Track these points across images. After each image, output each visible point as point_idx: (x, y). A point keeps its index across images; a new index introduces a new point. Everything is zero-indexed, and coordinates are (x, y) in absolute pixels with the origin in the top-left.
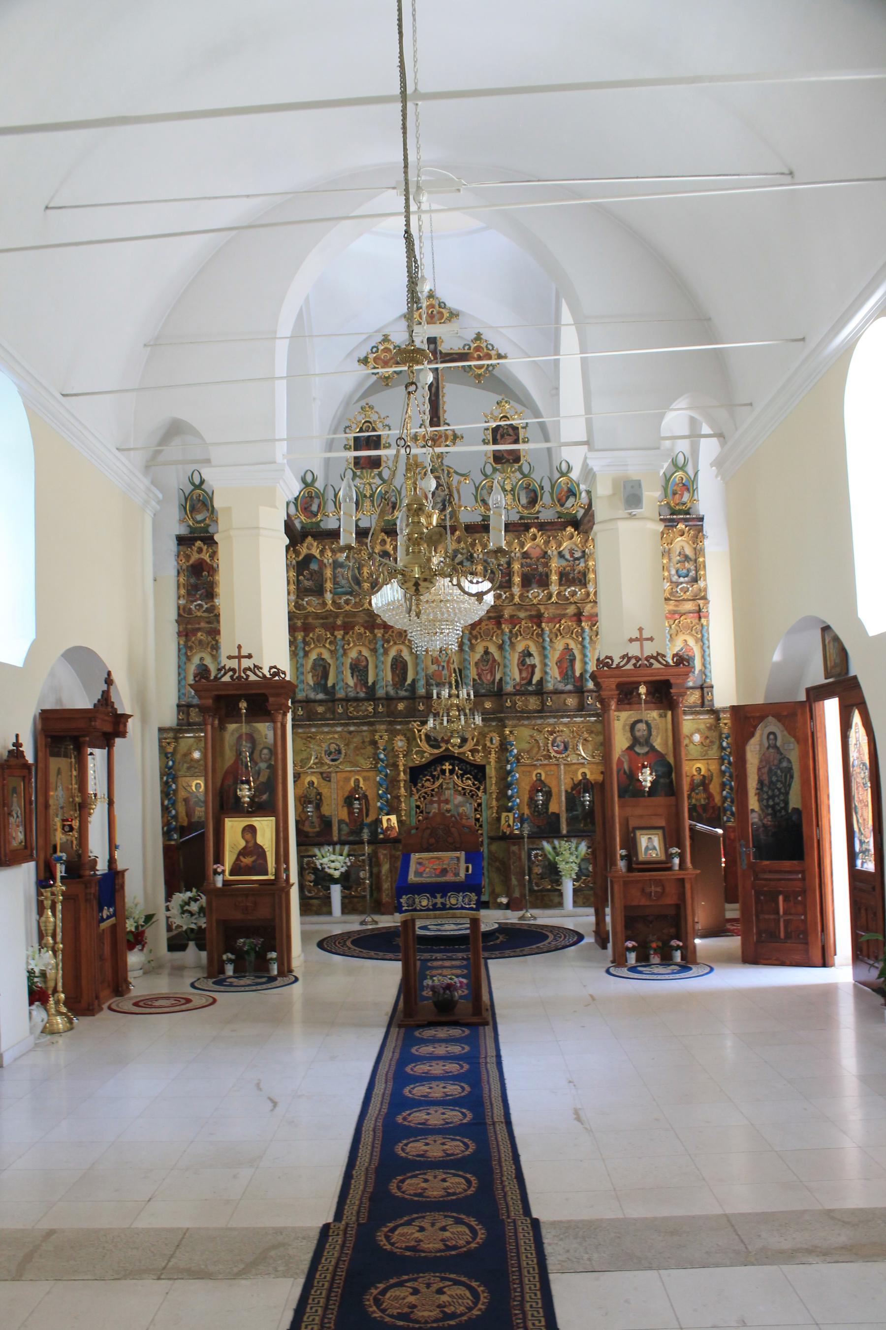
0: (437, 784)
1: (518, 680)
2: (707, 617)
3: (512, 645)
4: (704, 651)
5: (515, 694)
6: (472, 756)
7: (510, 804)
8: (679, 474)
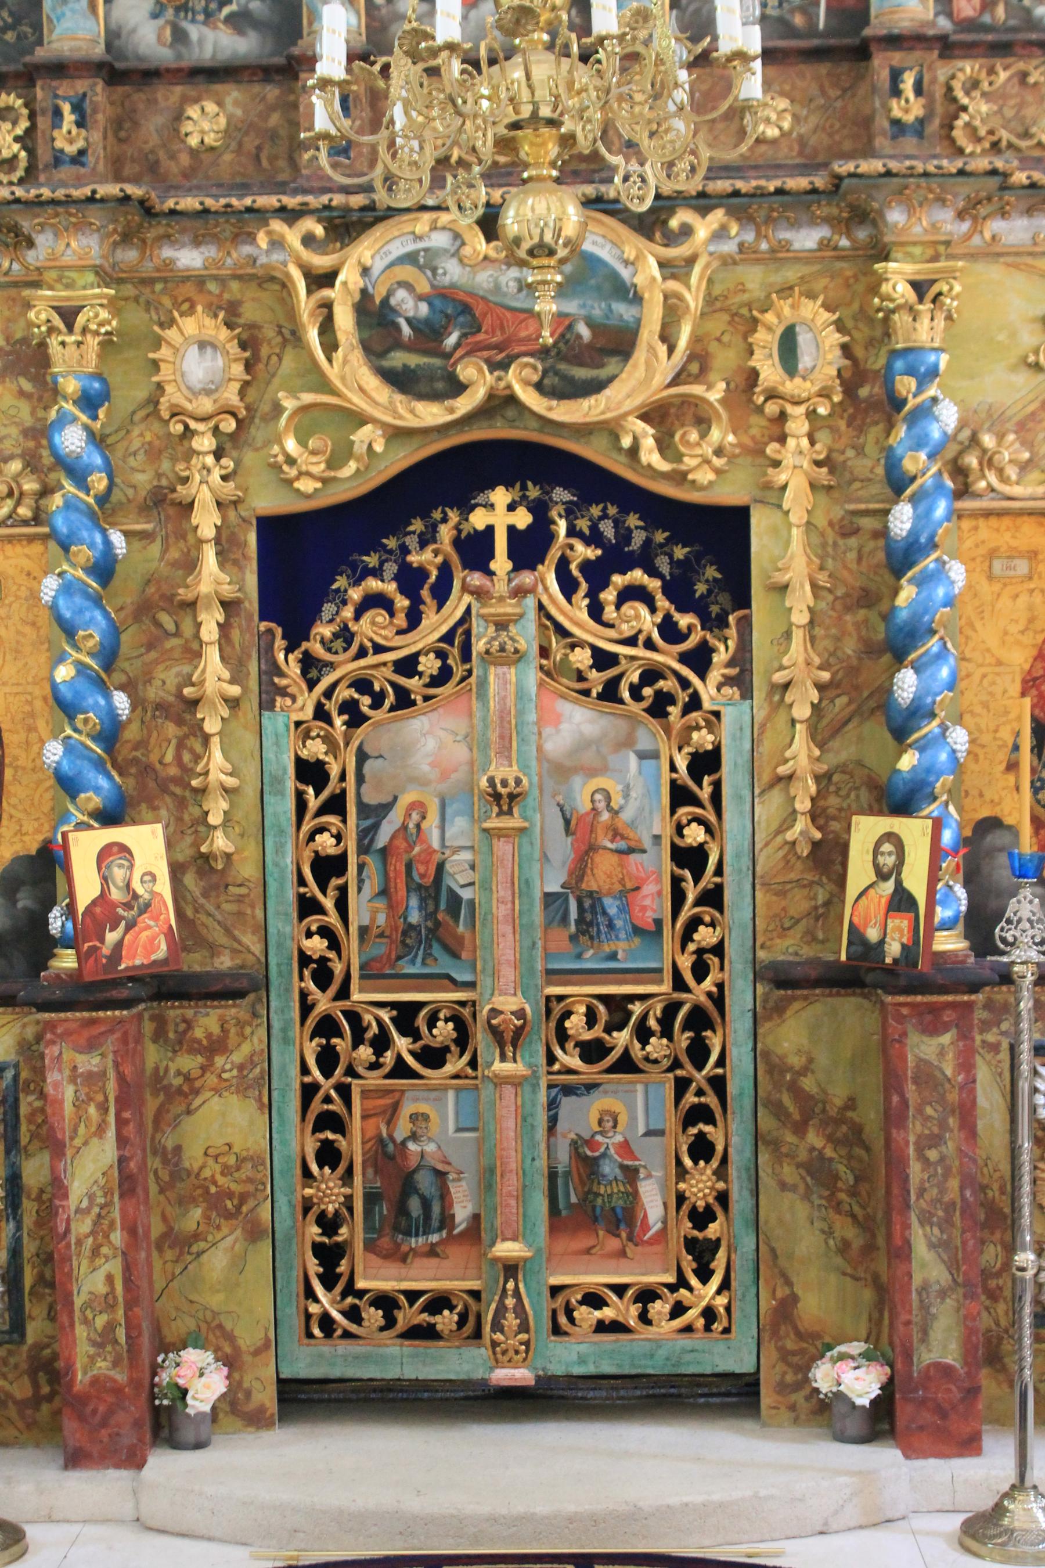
6: (664, 445)
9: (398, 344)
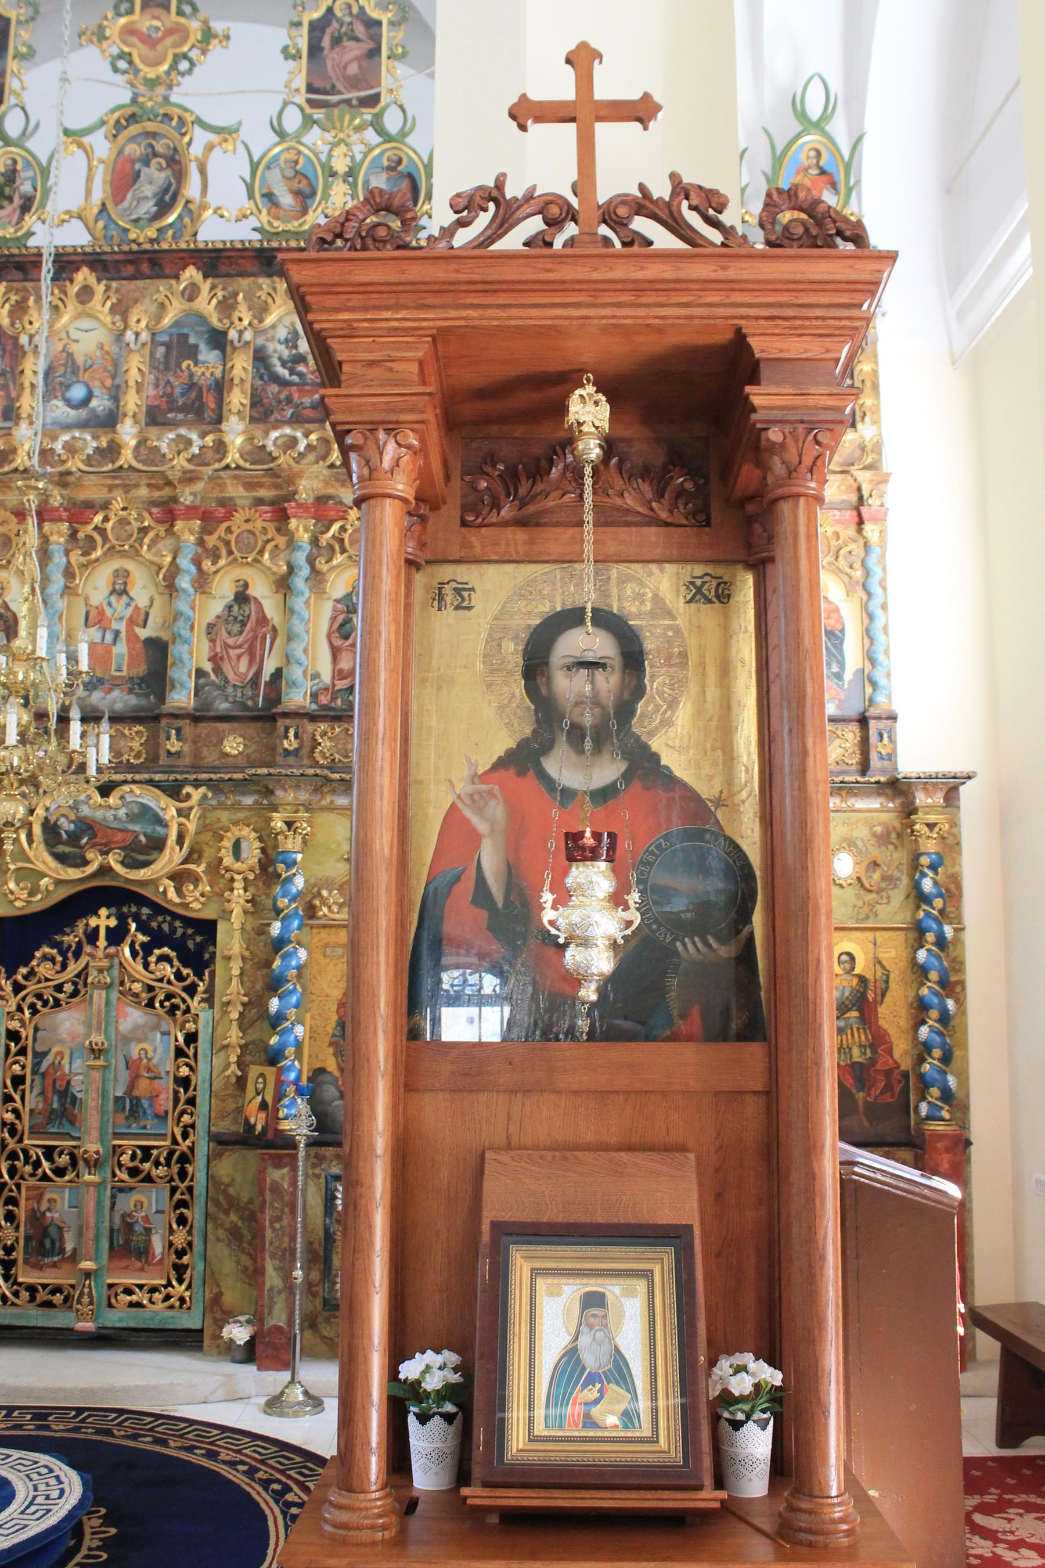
0: (73, 968)
1: (326, 677)
2: (880, 519)
3: (317, 577)
4: (871, 617)
5: (313, 718)
6: (179, 892)
7: (274, 1040)
8: (811, 139)
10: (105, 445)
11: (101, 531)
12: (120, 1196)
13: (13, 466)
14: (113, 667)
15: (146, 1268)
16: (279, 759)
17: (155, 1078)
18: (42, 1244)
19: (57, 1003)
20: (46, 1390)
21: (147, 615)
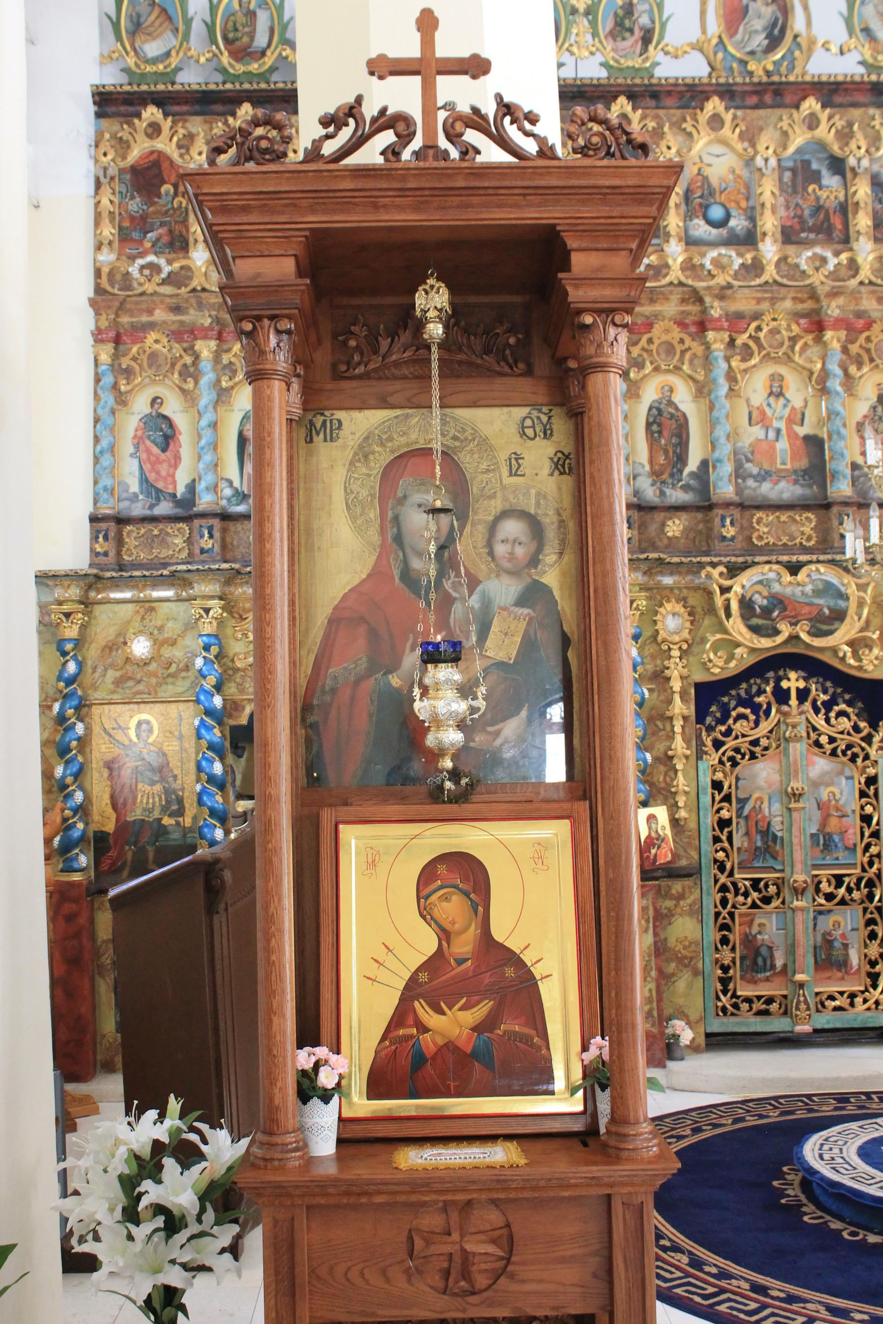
6: (855, 654)
9: (754, 615)
10: (750, 261)
11: (756, 340)
12: (821, 918)
13: (667, 280)
14: (778, 462)
15: (846, 977)
16: (718, 546)
17: (843, 816)
18: (755, 963)
19: (753, 756)
20: (826, 1079)
21: (803, 415)
